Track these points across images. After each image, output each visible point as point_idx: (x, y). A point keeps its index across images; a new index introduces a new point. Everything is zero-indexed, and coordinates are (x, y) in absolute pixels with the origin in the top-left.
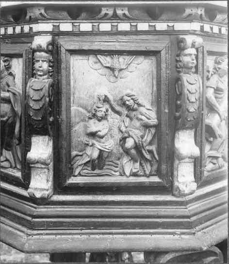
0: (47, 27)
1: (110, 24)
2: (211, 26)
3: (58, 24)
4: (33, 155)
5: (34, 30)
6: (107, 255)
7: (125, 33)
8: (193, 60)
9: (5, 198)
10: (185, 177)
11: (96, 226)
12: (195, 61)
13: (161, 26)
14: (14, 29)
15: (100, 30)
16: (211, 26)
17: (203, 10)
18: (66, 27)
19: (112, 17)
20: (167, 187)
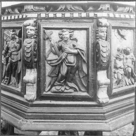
0: (35, 15)
2: (108, 13)
5: (28, 17)
8: (105, 35)
9: (3, 99)
10: (102, 95)
11: (51, 118)
13: (92, 15)
15: (49, 17)
16: (130, 15)
19: (64, 9)
20: (94, 98)
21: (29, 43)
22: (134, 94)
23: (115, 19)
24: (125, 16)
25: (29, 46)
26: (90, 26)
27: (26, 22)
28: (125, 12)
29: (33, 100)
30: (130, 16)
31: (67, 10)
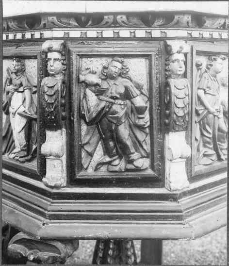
0: (59, 33)
1: (159, 31)
2: (211, 33)
3: (118, 31)
4: (45, 149)
6: (111, 242)
7: (141, 39)
9: (6, 185)
12: (184, 66)
13: (156, 33)
14: (15, 36)
15: (153, 36)
16: (220, 33)
17: (190, 17)
18: (75, 33)
19: (113, 23)
21: (55, 82)
22: (227, 175)
23: (202, 39)
24: (221, 35)
25: (51, 92)
26: (152, 49)
27: (45, 46)
28: (217, 28)
29: (60, 186)
30: (212, 35)
31: (118, 25)
